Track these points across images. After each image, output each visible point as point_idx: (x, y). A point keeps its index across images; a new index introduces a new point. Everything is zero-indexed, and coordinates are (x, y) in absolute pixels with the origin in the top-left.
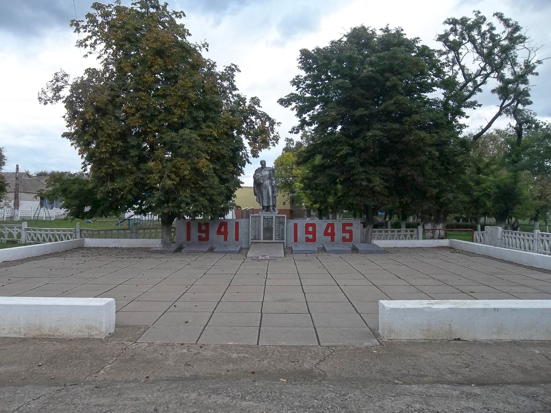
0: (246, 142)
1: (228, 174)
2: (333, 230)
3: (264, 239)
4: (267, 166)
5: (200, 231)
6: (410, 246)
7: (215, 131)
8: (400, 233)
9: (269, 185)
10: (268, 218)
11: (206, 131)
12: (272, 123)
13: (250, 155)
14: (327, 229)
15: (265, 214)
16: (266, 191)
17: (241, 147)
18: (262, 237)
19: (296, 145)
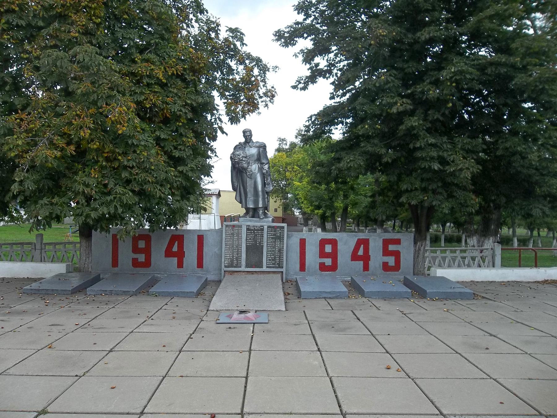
0: (219, 102)
1: (184, 150)
2: (366, 250)
3: (247, 266)
4: (254, 139)
5: (136, 250)
6: (498, 279)
7: (160, 68)
8: (465, 255)
9: (257, 171)
10: (255, 230)
11: (141, 68)
12: (264, 69)
13: (225, 118)
14: (356, 248)
15: (251, 221)
16: (253, 181)
17: (210, 107)
18: (243, 263)
19: (290, 145)
